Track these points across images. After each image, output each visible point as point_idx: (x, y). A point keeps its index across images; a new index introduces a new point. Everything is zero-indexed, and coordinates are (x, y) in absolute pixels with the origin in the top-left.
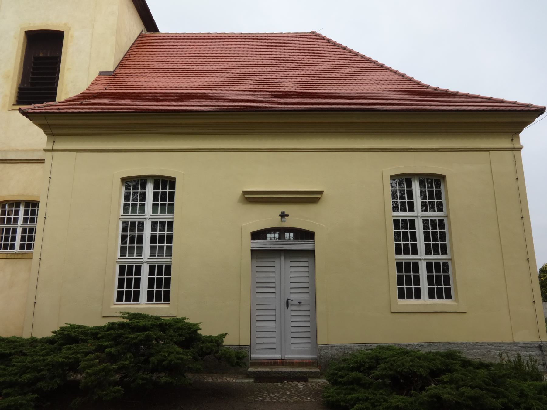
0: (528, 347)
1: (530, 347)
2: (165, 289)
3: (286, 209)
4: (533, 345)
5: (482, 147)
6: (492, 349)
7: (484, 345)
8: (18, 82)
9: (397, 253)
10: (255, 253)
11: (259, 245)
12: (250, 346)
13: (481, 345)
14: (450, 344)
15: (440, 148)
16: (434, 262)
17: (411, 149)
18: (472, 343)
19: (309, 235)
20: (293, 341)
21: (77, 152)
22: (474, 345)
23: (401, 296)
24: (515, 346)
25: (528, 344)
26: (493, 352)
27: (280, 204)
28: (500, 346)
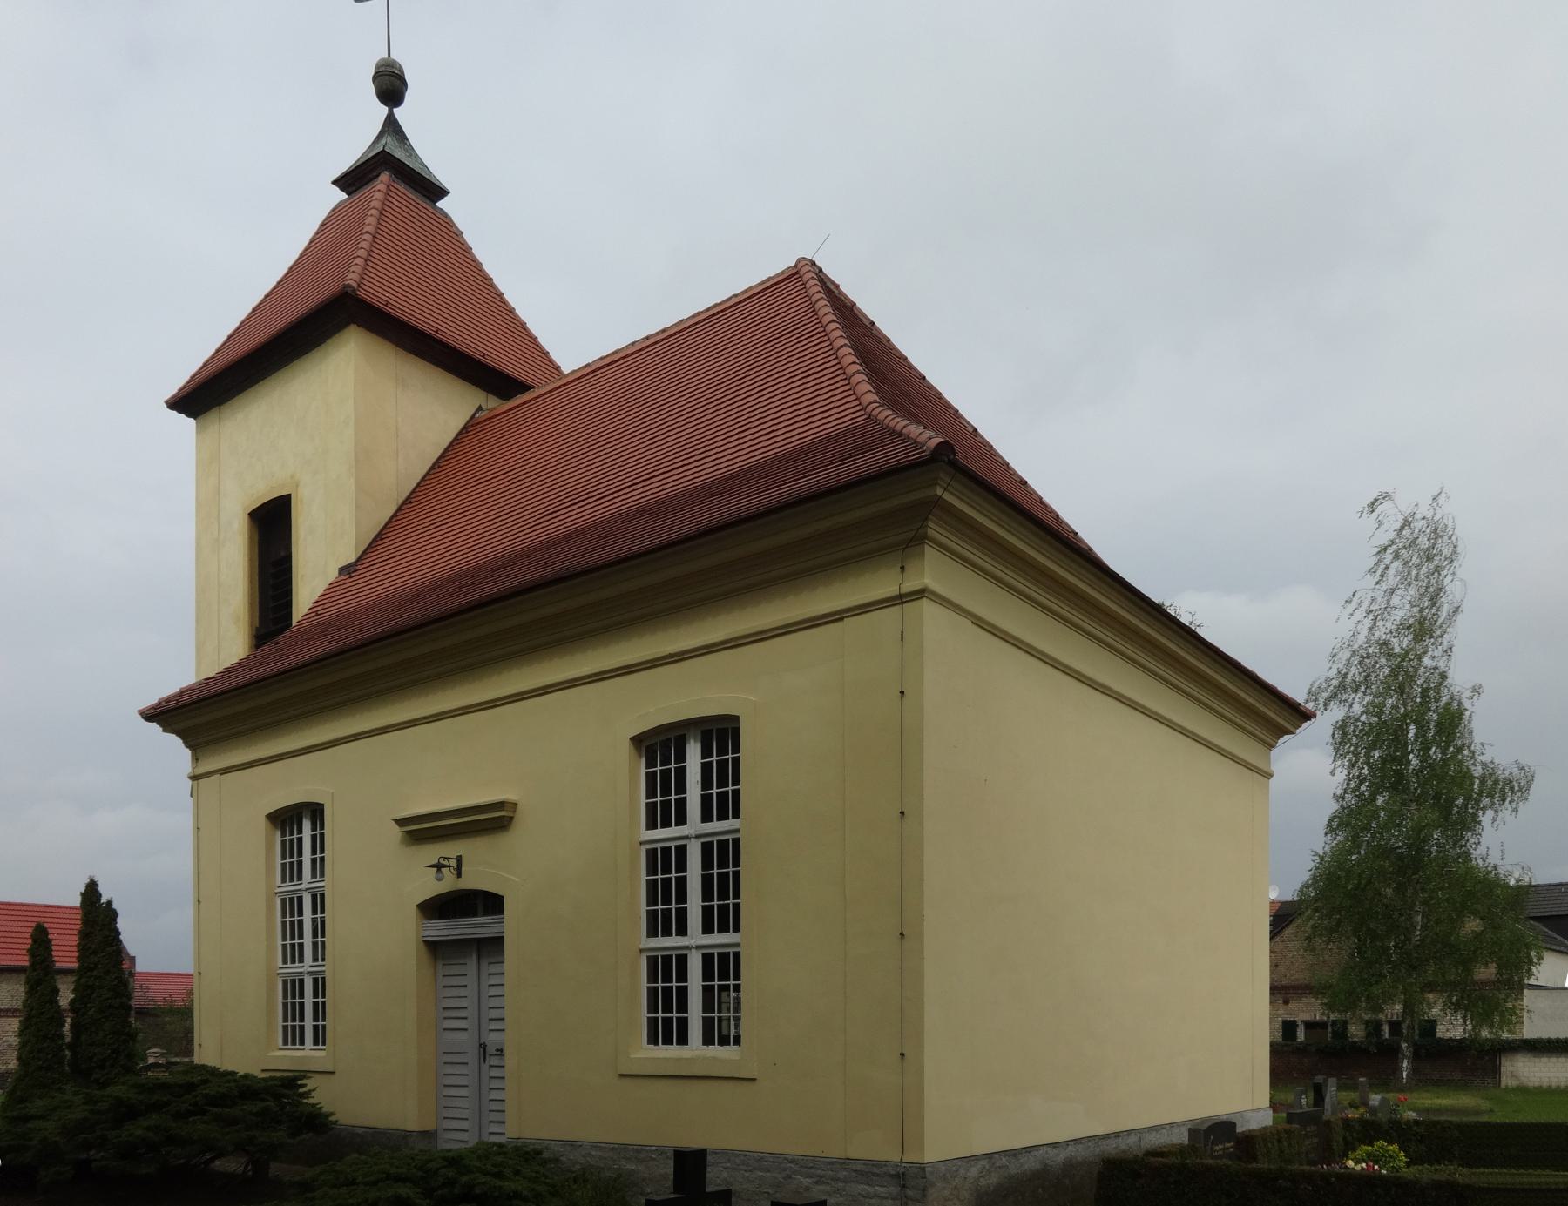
0: (874, 1174)
1: (878, 1175)
2: (660, 1012)
3: (450, 849)
4: (884, 1169)
6: (795, 1172)
7: (780, 1160)
8: (251, 624)
11: (441, 930)
12: (436, 1131)
13: (775, 1160)
17: (671, 656)
18: (756, 1155)
19: (491, 903)
21: (221, 774)
23: (653, 1040)
26: (795, 1179)
27: (443, 841)
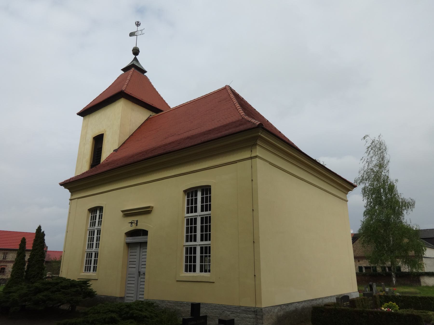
3: (135, 219)
5: (232, 161)
7: (221, 306)
8: (90, 163)
9: (186, 242)
10: (129, 245)
11: (131, 240)
14: (203, 304)
15: (209, 167)
16: (204, 247)
17: (194, 171)
19: (145, 233)
20: (132, 295)
22: (215, 306)
24: (240, 309)
25: (247, 308)
28: (230, 309)
